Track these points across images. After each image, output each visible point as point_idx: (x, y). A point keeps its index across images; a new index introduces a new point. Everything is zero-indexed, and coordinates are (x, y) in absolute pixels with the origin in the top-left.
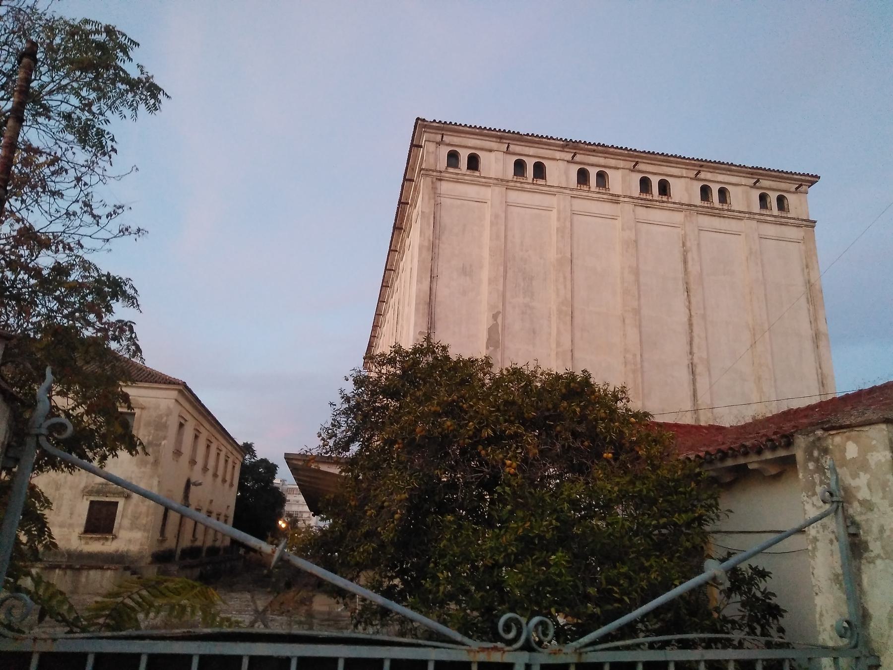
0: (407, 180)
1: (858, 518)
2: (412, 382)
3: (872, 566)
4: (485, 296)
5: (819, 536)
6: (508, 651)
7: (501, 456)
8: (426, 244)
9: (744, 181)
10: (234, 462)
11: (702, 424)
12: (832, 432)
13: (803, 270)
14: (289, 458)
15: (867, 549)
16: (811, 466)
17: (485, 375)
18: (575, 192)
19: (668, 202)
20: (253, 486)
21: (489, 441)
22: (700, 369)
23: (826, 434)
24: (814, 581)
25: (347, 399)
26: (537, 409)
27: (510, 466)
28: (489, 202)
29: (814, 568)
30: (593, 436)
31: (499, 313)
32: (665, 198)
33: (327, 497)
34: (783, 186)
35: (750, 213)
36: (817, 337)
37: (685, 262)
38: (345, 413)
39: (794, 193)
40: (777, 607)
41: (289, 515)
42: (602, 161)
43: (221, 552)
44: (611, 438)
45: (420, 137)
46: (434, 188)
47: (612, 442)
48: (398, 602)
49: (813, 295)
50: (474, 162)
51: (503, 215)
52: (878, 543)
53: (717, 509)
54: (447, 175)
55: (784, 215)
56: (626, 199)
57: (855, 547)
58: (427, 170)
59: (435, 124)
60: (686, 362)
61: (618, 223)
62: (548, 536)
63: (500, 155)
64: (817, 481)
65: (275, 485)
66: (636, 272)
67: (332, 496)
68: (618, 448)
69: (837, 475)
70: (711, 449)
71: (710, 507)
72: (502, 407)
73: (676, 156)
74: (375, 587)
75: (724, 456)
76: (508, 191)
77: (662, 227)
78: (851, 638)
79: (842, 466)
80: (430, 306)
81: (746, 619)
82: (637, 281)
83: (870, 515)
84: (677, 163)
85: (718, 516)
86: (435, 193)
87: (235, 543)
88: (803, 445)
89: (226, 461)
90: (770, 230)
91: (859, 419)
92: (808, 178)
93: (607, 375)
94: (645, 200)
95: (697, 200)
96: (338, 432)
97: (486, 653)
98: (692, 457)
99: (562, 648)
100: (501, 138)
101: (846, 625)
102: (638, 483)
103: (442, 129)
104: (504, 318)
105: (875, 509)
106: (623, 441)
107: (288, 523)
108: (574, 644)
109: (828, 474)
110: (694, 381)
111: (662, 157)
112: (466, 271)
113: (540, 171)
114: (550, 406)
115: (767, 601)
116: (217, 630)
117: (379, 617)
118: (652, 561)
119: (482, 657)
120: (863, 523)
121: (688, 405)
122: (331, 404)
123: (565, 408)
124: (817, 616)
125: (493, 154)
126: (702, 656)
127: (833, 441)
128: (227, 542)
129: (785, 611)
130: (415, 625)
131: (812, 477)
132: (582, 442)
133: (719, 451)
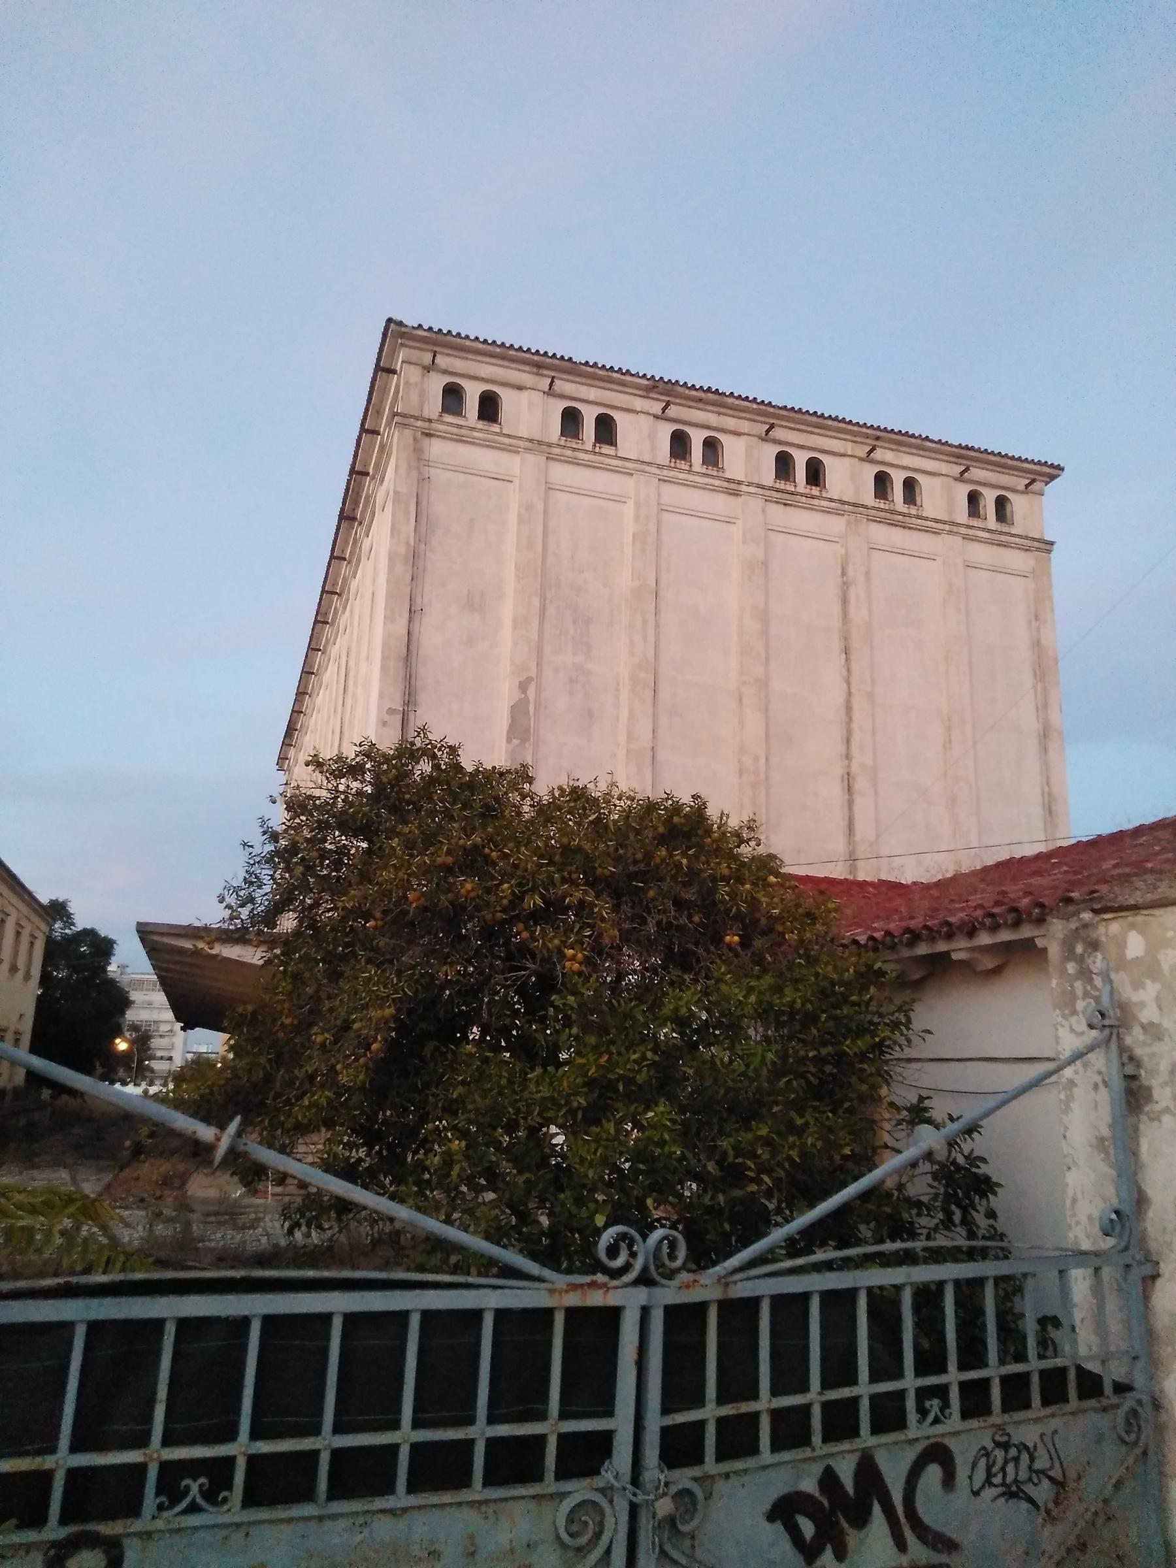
0: (367, 430)
1: (1138, 1052)
2: (394, 809)
3: (1156, 1123)
4: (506, 648)
5: (1078, 1079)
6: (616, 1288)
7: (556, 942)
8: (402, 550)
9: (944, 468)
10: (18, 924)
11: (861, 877)
12: (1106, 916)
13: (1030, 623)
14: (145, 932)
15: (1149, 1098)
16: (1071, 968)
17: (523, 798)
18: (665, 472)
19: (820, 498)
20: (69, 976)
21: (536, 917)
22: (860, 784)
23: (1097, 918)
24: (1066, 1149)
25: (274, 837)
26: (618, 860)
27: (573, 958)
28: (516, 482)
29: (1066, 1128)
30: (708, 904)
31: (529, 680)
32: (815, 491)
33: (240, 1010)
34: (1005, 480)
35: (953, 523)
36: (1045, 735)
37: (845, 602)
38: (269, 860)
39: (1022, 492)
40: (987, 1179)
41: (135, 1028)
42: (712, 418)
43: (8, 1098)
44: (738, 910)
45: (393, 352)
46: (418, 451)
47: (739, 917)
48: (365, 1187)
49: (1043, 668)
50: (489, 407)
51: (540, 506)
52: (1168, 1090)
53: (908, 1029)
54: (442, 427)
55: (1005, 529)
56: (752, 489)
57: (1133, 1095)
58: (404, 416)
59: (421, 333)
60: (838, 770)
61: (737, 530)
62: (640, 1079)
63: (537, 397)
64: (1079, 992)
65: (111, 975)
66: (763, 616)
67: (250, 1008)
68: (750, 926)
69: (1111, 981)
70: (892, 926)
71: (895, 1025)
72: (557, 858)
73: (836, 419)
74: (330, 1166)
75: (915, 937)
76: (552, 464)
77: (810, 538)
78: (1121, 1237)
79: (1117, 970)
80: (407, 661)
81: (941, 1198)
82: (765, 633)
83: (1157, 1047)
84: (838, 430)
85: (909, 1041)
86: (419, 459)
87: (35, 1079)
88: (1060, 935)
89: (18, 934)
90: (982, 553)
91: (1149, 897)
92: (1047, 470)
93: (727, 805)
94: (782, 491)
95: (868, 496)
96: (258, 894)
97: (579, 1292)
98: (862, 939)
99: (697, 1277)
100: (539, 366)
101: (1114, 1216)
102: (788, 991)
103: (435, 344)
104: (539, 690)
105: (1167, 1039)
106: (757, 915)
107: (132, 1042)
108: (717, 1268)
109: (1098, 981)
110: (850, 804)
111: (814, 419)
112: (475, 603)
113: (606, 429)
114: (639, 856)
115: (974, 1170)
116: (120, 1277)
117: (333, 1214)
118: (809, 1117)
119: (573, 1300)
120: (1146, 1059)
121: (839, 846)
122: (245, 844)
123: (663, 860)
124: (1068, 1202)
125: (524, 395)
126: (909, 1276)
127: (1107, 930)
128: (20, 1077)
129: (999, 1185)
130: (398, 1225)
131: (1071, 986)
132: (690, 917)
133: (908, 930)
